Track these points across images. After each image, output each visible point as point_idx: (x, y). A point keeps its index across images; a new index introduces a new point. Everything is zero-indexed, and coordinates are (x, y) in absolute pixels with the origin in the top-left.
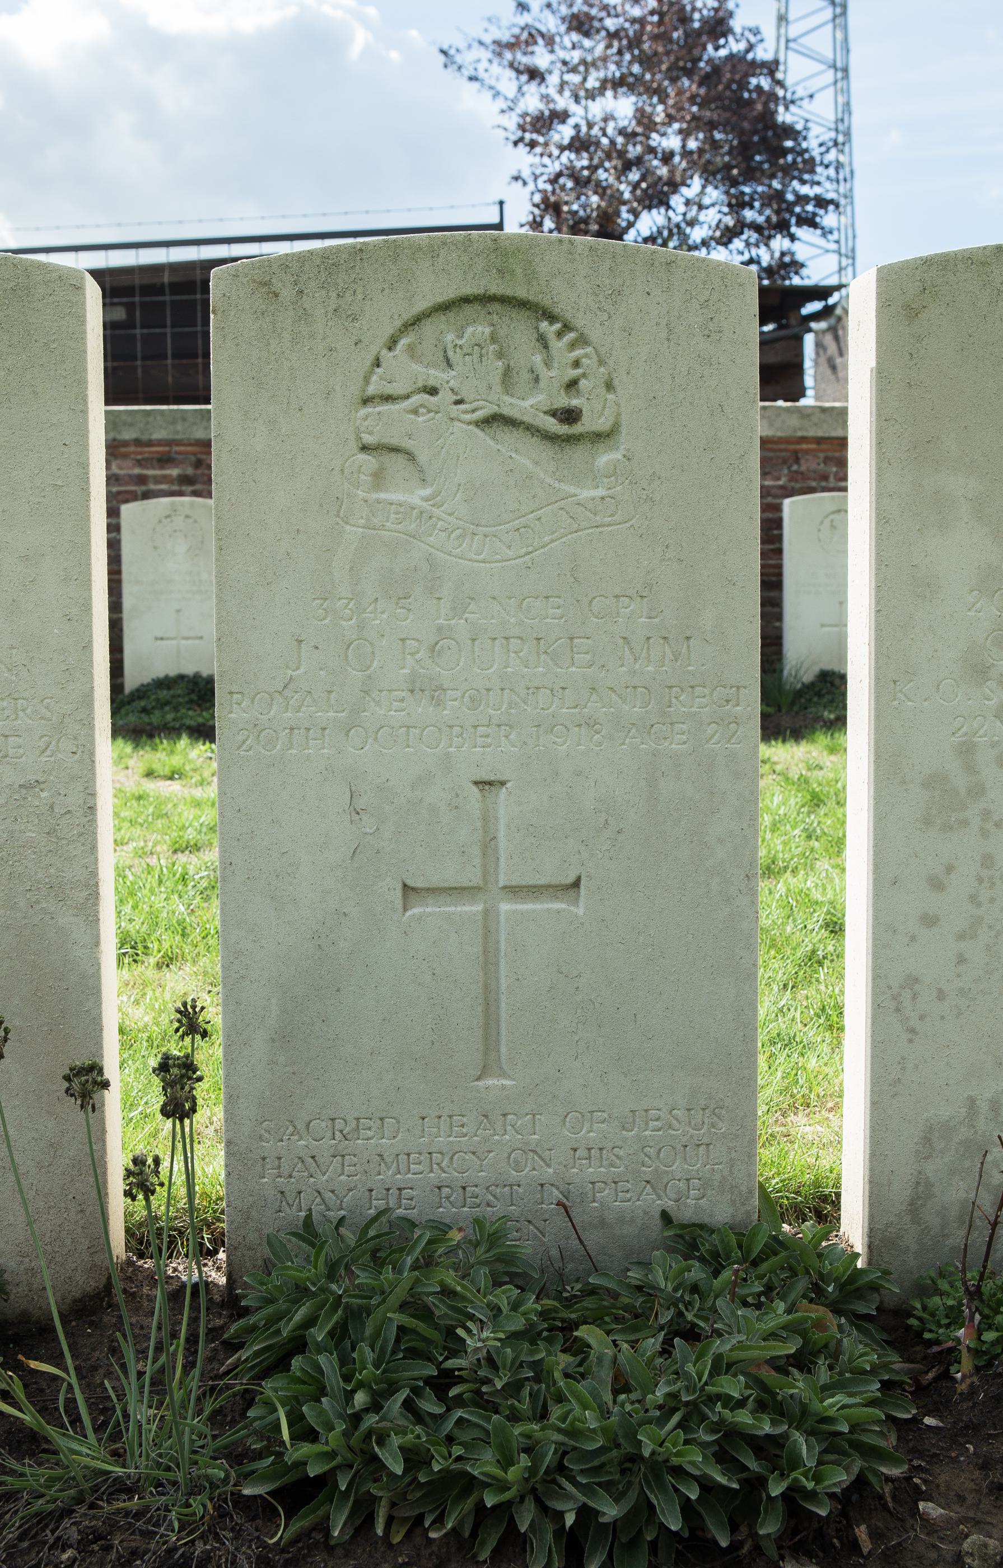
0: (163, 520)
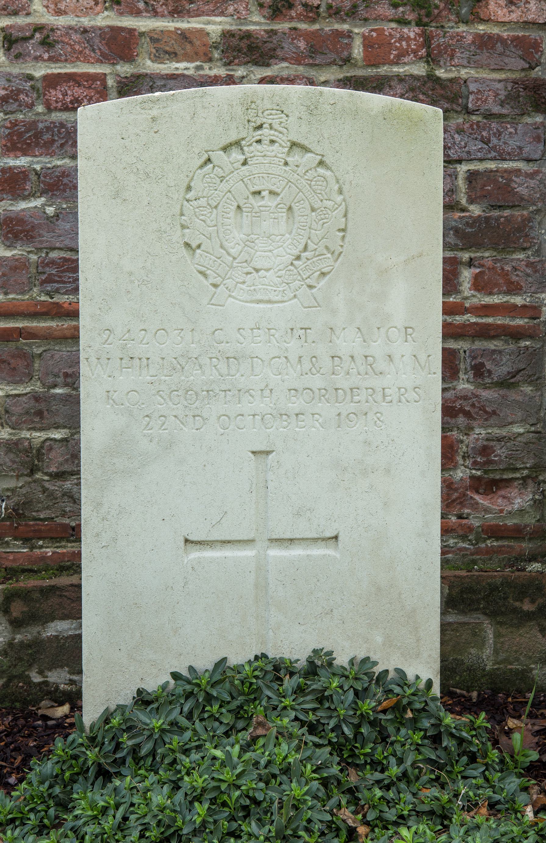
0: (218, 156)
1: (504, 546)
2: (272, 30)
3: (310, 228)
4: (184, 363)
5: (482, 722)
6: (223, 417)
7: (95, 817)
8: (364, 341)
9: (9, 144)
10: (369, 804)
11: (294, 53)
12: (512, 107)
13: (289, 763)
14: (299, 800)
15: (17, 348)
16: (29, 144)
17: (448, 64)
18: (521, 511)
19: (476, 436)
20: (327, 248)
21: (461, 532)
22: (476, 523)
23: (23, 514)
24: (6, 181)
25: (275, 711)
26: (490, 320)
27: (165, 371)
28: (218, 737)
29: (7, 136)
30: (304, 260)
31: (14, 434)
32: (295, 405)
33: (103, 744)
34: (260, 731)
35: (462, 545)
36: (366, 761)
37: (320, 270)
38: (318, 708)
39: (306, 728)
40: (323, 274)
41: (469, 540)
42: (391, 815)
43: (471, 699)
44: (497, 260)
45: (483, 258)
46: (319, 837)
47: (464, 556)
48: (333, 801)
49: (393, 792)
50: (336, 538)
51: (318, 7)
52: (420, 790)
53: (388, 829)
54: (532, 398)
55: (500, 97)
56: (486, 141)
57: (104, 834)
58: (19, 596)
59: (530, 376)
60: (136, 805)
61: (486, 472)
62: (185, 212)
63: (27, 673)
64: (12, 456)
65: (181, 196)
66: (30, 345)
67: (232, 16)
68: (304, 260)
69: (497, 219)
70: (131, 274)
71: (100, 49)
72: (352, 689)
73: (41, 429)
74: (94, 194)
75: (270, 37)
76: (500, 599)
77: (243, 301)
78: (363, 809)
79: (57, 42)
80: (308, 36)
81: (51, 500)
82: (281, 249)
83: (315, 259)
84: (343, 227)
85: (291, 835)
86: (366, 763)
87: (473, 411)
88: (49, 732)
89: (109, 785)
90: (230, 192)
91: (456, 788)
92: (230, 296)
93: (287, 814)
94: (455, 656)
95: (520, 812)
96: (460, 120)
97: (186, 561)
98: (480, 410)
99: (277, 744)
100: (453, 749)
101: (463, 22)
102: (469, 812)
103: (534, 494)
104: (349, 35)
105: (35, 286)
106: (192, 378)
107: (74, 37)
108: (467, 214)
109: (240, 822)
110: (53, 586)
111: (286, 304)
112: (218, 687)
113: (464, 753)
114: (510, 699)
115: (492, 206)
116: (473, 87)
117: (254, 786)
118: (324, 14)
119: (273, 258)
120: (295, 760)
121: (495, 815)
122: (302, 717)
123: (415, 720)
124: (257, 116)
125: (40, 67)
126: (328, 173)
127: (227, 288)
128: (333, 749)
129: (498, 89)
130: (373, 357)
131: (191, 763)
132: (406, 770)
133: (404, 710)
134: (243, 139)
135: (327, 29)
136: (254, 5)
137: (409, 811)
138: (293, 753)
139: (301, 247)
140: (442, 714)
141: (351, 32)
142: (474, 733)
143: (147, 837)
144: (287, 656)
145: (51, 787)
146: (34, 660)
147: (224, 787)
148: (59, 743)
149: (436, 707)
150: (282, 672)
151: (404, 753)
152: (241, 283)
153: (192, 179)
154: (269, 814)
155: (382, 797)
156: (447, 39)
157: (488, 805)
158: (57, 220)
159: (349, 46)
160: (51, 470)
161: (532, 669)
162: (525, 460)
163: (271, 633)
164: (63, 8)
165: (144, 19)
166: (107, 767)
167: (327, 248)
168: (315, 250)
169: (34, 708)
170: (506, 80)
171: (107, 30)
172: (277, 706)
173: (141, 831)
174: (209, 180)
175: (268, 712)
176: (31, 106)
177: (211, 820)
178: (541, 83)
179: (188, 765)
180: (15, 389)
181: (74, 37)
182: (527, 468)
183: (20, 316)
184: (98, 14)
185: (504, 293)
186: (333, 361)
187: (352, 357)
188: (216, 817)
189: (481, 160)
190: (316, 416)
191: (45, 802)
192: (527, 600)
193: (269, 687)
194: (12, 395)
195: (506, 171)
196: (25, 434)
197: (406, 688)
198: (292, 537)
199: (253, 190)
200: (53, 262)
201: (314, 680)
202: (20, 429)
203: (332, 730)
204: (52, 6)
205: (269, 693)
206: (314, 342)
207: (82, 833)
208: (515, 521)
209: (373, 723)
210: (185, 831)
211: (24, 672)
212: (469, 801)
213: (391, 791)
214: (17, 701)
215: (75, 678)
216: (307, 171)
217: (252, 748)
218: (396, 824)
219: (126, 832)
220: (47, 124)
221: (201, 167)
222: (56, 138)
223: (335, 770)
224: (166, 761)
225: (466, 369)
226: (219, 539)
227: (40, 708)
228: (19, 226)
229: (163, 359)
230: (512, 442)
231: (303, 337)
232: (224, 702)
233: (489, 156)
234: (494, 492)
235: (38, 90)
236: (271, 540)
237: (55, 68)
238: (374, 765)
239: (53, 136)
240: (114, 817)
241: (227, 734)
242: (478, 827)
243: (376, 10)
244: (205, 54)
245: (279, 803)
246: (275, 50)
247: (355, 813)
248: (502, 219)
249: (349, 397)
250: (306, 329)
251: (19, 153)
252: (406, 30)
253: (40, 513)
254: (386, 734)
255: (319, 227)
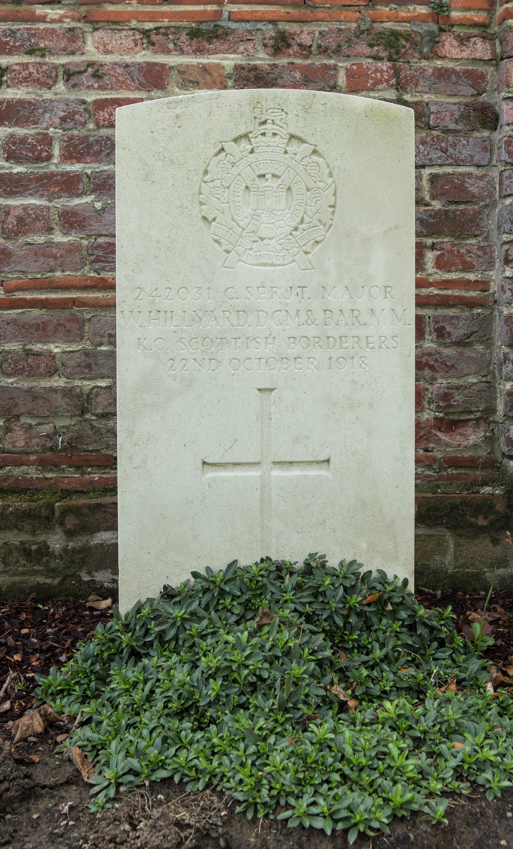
0: (230, 146)
1: (461, 474)
2: (274, 64)
3: (306, 204)
4: (202, 316)
5: (449, 614)
6: (234, 360)
7: (127, 690)
8: (351, 298)
9: (66, 154)
10: (357, 682)
11: (291, 82)
12: (464, 124)
13: (290, 647)
14: (298, 678)
15: (71, 314)
16: (82, 154)
17: (414, 91)
18: (475, 446)
19: (439, 385)
20: (320, 221)
21: (427, 463)
22: (439, 455)
23: (76, 447)
24: (64, 182)
25: (277, 604)
26: (449, 292)
27: (186, 322)
28: (230, 625)
29: (65, 148)
30: (301, 231)
31: (69, 383)
32: (294, 350)
33: (135, 630)
34: (265, 621)
35: (427, 473)
36: (354, 646)
37: (314, 239)
38: (314, 602)
39: (303, 618)
40: (317, 242)
41: (434, 469)
42: (376, 690)
43: (436, 596)
44: (454, 244)
45: (443, 242)
46: (315, 709)
47: (429, 481)
48: (328, 679)
49: (377, 672)
50: (328, 461)
51: (310, 46)
52: (399, 670)
53: (373, 702)
54: (483, 354)
55: (455, 116)
56: (445, 151)
57: (134, 704)
58: (72, 512)
59: (482, 337)
60: (162, 681)
61: (447, 414)
62: (202, 192)
63: (78, 573)
64: (67, 400)
65: (200, 178)
66: (81, 312)
67: (243, 53)
68: (300, 230)
69: (454, 212)
70: (158, 242)
71: (138, 80)
72: (342, 586)
73: (90, 379)
74: (128, 177)
75: (272, 69)
76: (459, 516)
77: (251, 264)
78: (352, 686)
79: (105, 74)
80: (302, 69)
81: (98, 435)
82: (282, 221)
83: (310, 230)
84: (332, 203)
85: (292, 708)
86: (354, 647)
87: (436, 365)
88: (95, 620)
89: (140, 664)
90: (240, 175)
91: (428, 668)
92: (240, 260)
93: (288, 691)
94: (423, 562)
95: (482, 687)
96: (424, 134)
97: (203, 480)
98: (442, 364)
99: (279, 631)
100: (426, 636)
101: (425, 59)
102: (440, 688)
103: (485, 431)
104: (335, 68)
105: (86, 265)
106: (209, 327)
107: (118, 70)
108: (430, 208)
109: (248, 696)
110: (99, 504)
111: (286, 266)
112: (231, 584)
113: (435, 639)
114: (467, 597)
115: (450, 202)
116: (433, 109)
117: (260, 666)
118: (315, 52)
119: (275, 229)
120: (294, 644)
121: (462, 690)
122: (300, 608)
123: (394, 612)
124: (262, 114)
125: (92, 94)
126: (321, 160)
127: (237, 253)
128: (326, 635)
129: (453, 110)
130: (359, 311)
131: (207, 646)
132: (388, 653)
133: (385, 604)
134: (250, 132)
135: (317, 63)
136: (259, 45)
137: (391, 687)
138: (293, 638)
139: (298, 220)
140: (416, 607)
141: (337, 66)
142: (443, 622)
143: (170, 708)
144: (287, 559)
145: (92, 664)
146: (84, 563)
147: (234, 667)
148: (99, 628)
149: (411, 601)
150: (284, 572)
151: (385, 639)
152: (249, 249)
153: (209, 165)
154: (273, 690)
155: (368, 676)
156: (412, 72)
157: (457, 682)
158: (104, 213)
159: (335, 76)
160: (98, 411)
161: (485, 572)
162: (478, 405)
163: (274, 539)
164: (110, 49)
165: (173, 57)
166: (138, 649)
167: (320, 221)
168: (310, 222)
169: (83, 602)
170: (459, 103)
171: (144, 65)
172: (280, 600)
173: (164, 703)
174: (222, 165)
175: (272, 605)
176: (84, 124)
177: (224, 694)
178: (487, 106)
179: (205, 648)
180: (70, 347)
181: (118, 70)
182: (479, 411)
183: (74, 289)
184: (137, 53)
185: (460, 271)
186: (325, 315)
187: (341, 311)
188: (228, 692)
189: (440, 165)
190: (311, 359)
191: (88, 677)
192: (480, 517)
193: (272, 584)
194: (67, 352)
195: (460, 174)
196: (78, 383)
197: (386, 585)
198: (291, 460)
199: (259, 173)
200: (100, 246)
201: (310, 579)
202: (73, 379)
203: (326, 620)
204: (102, 48)
205: (273, 590)
206: (309, 298)
207: (116, 703)
208: (470, 454)
209: (359, 614)
210: (202, 704)
211: (75, 572)
212: (440, 679)
213: (375, 671)
214: (70, 595)
215: (115, 577)
216: (303, 158)
217: (258, 634)
218: (380, 698)
219: (152, 703)
220: (97, 138)
221: (216, 155)
222: (104, 149)
223: (328, 653)
224: (187, 645)
225: (430, 331)
226: (231, 461)
227: (88, 601)
228: (74, 217)
229: (185, 312)
230: (468, 390)
231: (300, 294)
232: (235, 596)
233: (447, 162)
234: (453, 431)
235: (90, 112)
236: (274, 463)
237: (103, 94)
238: (361, 649)
239: (101, 147)
240: (143, 690)
241: (238, 623)
242: (449, 701)
243: (356, 49)
244: (221, 83)
245: (281, 680)
246: (276, 79)
247: (346, 689)
248: (458, 212)
249: (338, 344)
250: (302, 287)
251: (74, 161)
252: (380, 64)
253: (89, 446)
254: (370, 624)
255: (313, 204)
